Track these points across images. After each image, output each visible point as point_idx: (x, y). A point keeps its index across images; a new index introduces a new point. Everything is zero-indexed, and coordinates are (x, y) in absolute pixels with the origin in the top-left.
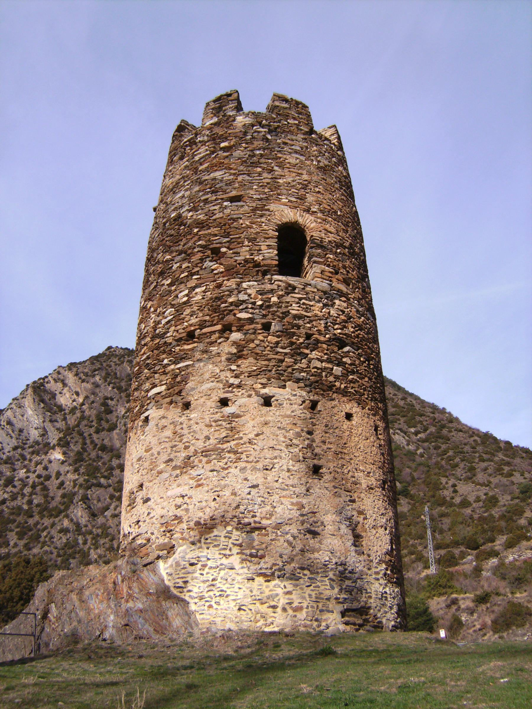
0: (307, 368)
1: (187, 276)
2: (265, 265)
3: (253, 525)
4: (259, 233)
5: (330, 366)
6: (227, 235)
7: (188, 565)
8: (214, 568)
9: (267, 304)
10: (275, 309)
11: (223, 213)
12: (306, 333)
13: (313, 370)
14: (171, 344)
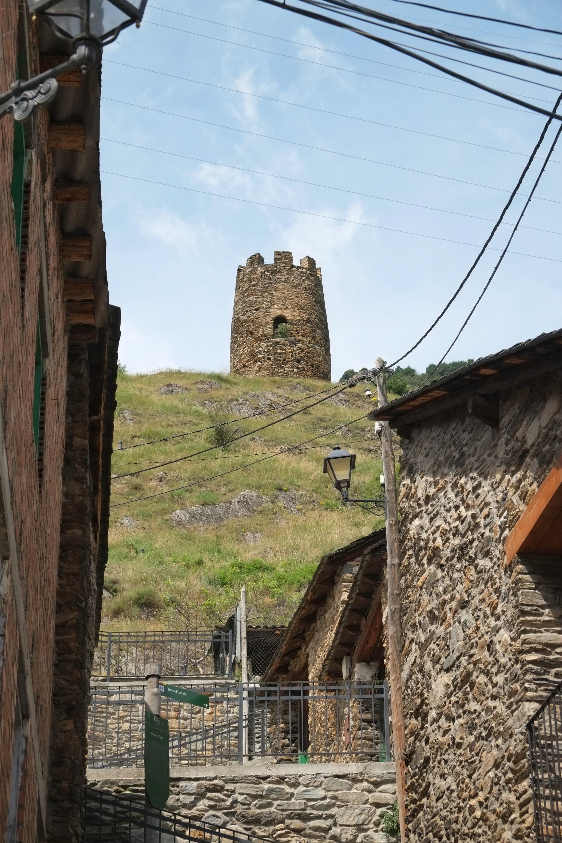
6: (255, 325)
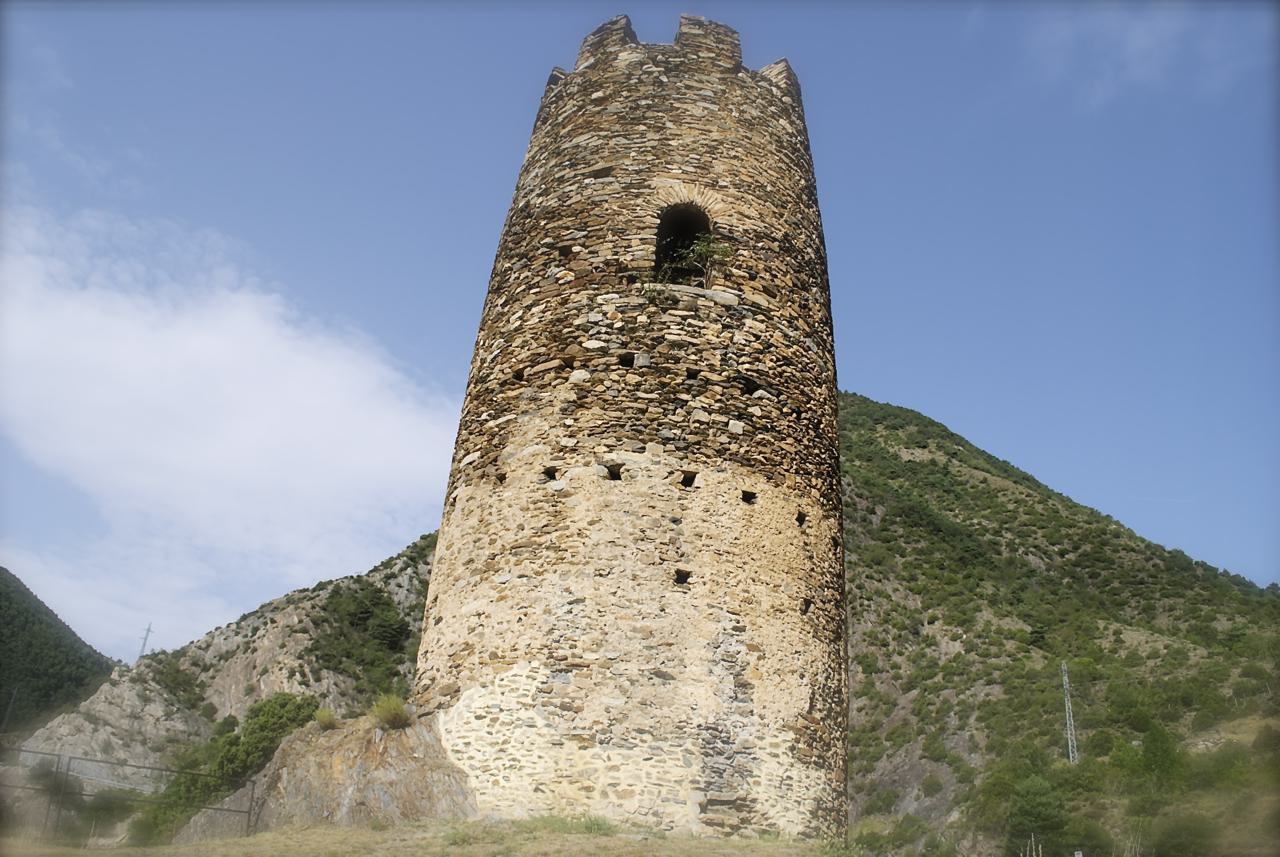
0: (683, 421)
1: (524, 290)
2: (634, 269)
3: (570, 660)
4: (631, 221)
5: (724, 419)
6: (584, 227)
7: (473, 719)
8: (508, 724)
9: (630, 326)
10: (641, 333)
11: (582, 195)
12: (688, 370)
13: (692, 426)
14: (493, 390)
